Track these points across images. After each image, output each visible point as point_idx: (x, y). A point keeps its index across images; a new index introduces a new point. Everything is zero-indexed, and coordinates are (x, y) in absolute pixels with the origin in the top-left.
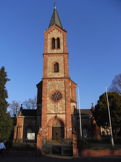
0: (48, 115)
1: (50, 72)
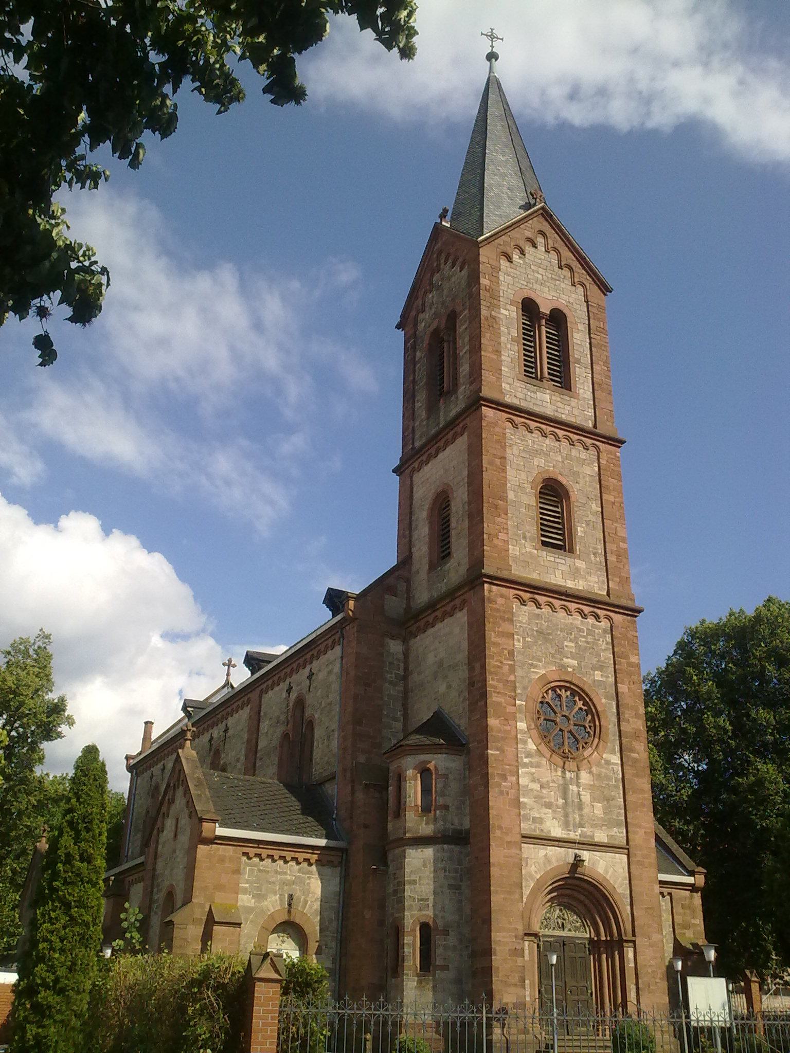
0: (529, 850)
1: (525, 538)
